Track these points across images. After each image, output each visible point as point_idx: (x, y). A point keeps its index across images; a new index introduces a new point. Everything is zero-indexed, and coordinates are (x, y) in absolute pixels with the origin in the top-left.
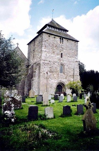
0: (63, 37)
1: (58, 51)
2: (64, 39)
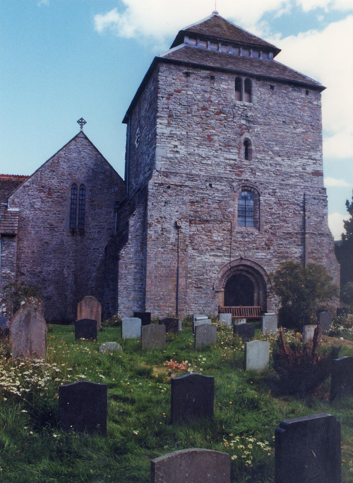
2: (255, 85)
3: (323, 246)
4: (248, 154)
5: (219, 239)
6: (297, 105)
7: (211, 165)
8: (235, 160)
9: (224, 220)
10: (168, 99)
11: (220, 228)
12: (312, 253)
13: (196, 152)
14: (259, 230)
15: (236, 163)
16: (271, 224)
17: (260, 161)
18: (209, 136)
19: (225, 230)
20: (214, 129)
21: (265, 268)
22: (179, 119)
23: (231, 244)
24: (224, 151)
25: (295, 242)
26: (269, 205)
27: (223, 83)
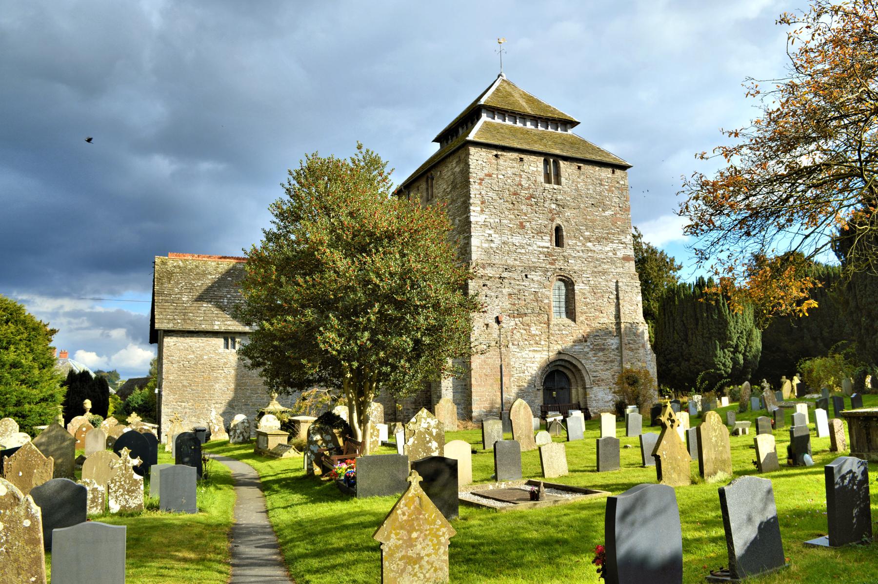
2: (561, 163)
8: (548, 248)
10: (480, 184)
14: (574, 320)
26: (584, 294)
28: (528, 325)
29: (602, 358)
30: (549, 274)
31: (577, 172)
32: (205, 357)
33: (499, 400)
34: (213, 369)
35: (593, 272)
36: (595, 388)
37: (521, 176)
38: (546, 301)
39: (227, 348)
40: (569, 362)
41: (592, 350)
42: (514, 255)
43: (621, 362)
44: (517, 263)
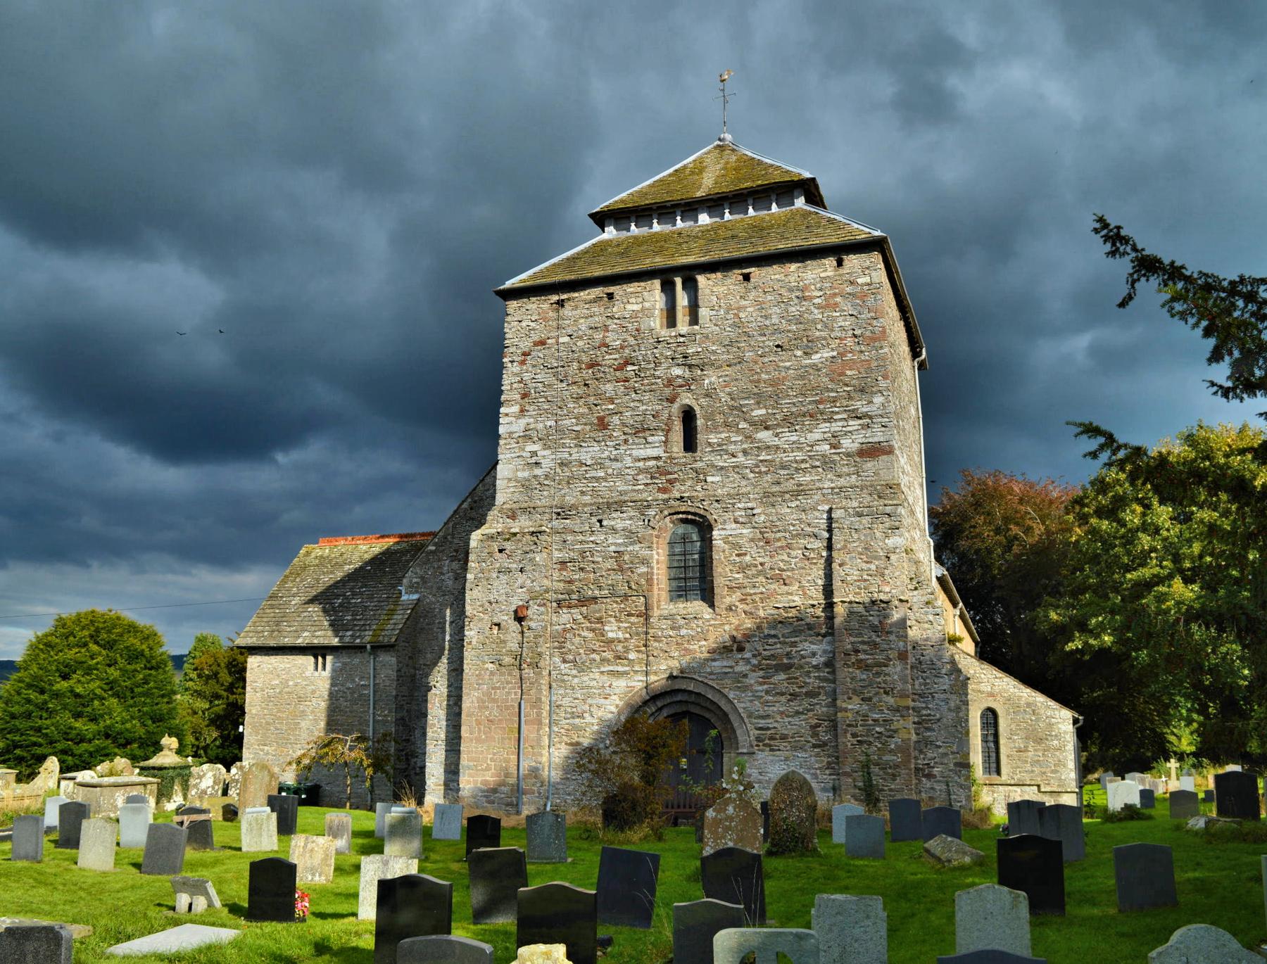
0: (690, 259)
1: (647, 397)
2: (701, 279)
3: (891, 633)
4: (690, 444)
5: (620, 635)
6: (811, 298)
7: (605, 479)
8: (658, 458)
9: (630, 592)
10: (523, 363)
11: (620, 612)
12: (857, 651)
13: (575, 456)
14: (712, 605)
15: (660, 464)
16: (744, 591)
17: (719, 449)
18: (601, 419)
19: (632, 615)
20: (611, 401)
21: (731, 696)
22: (542, 397)
23: (645, 646)
24: (634, 444)
25: (809, 629)
26: (736, 546)
27: (633, 300)
28: (599, 620)
29: (784, 687)
30: (652, 512)
31: (740, 289)
32: (291, 683)
33: (513, 770)
34: (300, 699)
35: (767, 495)
36: (760, 755)
37: (606, 328)
38: (643, 569)
39: (316, 669)
40: (699, 694)
41: (758, 667)
42: (580, 486)
43: (834, 696)
44: (587, 499)
